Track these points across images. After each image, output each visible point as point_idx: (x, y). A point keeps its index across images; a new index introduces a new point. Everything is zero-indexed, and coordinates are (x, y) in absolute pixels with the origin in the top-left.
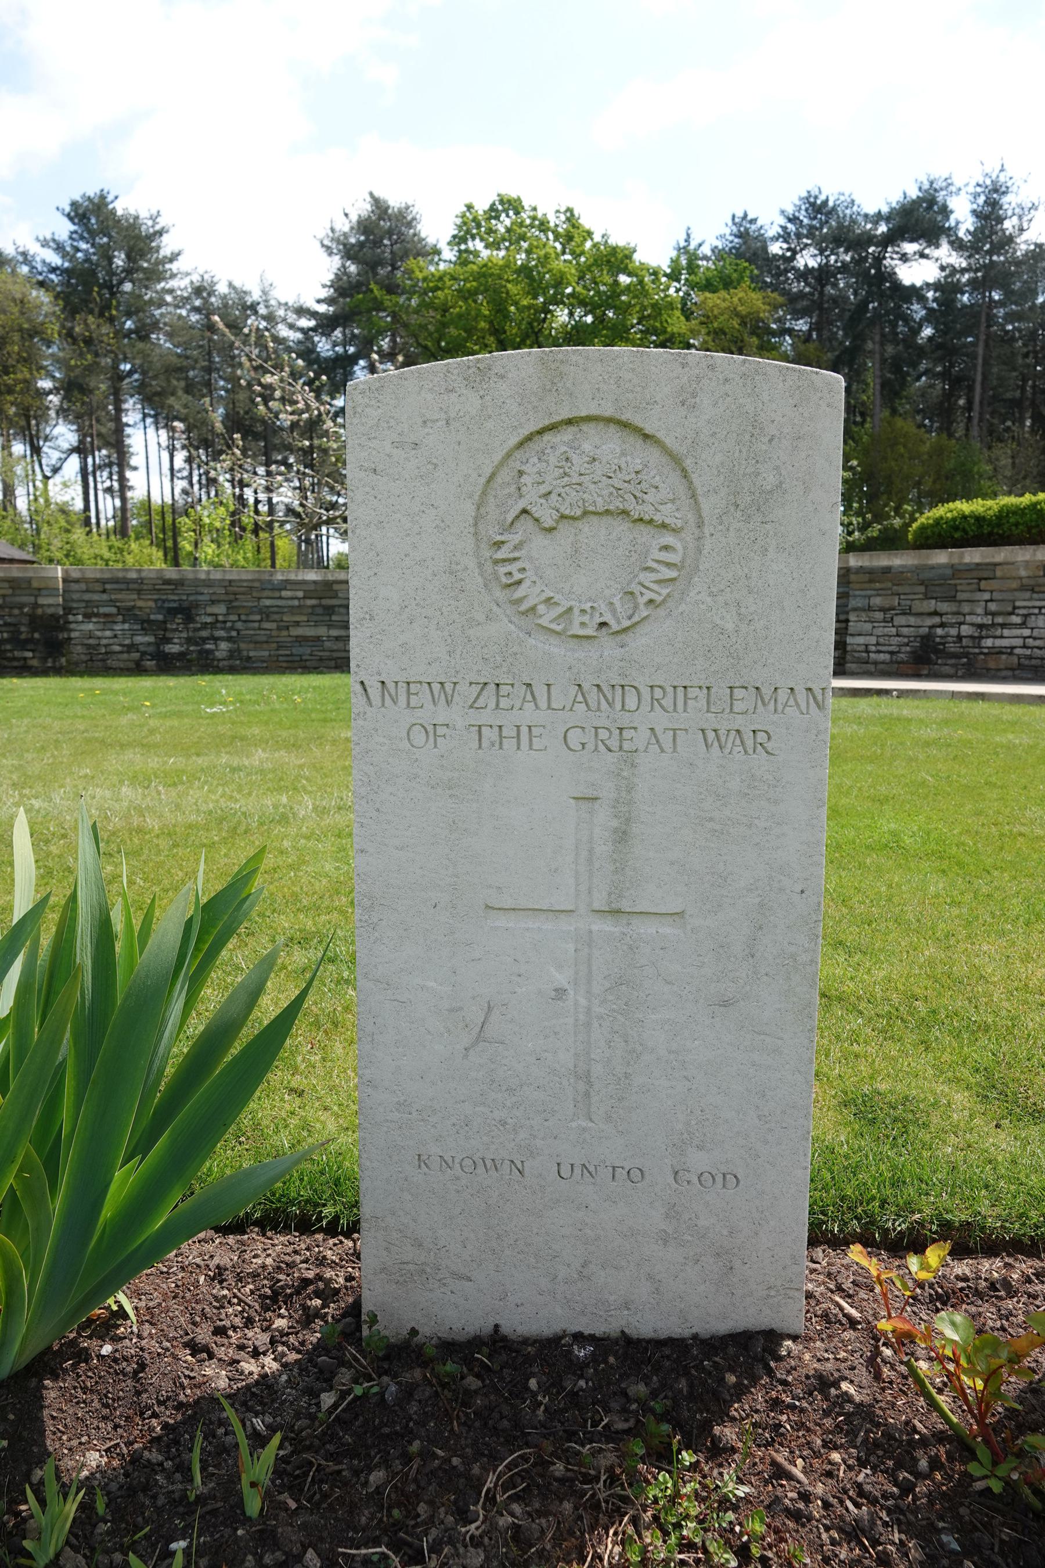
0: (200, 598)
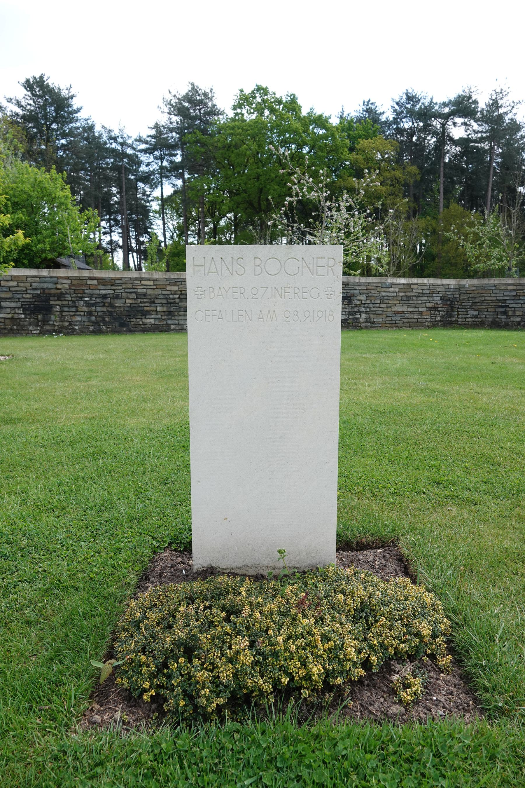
0: (355, 291)
